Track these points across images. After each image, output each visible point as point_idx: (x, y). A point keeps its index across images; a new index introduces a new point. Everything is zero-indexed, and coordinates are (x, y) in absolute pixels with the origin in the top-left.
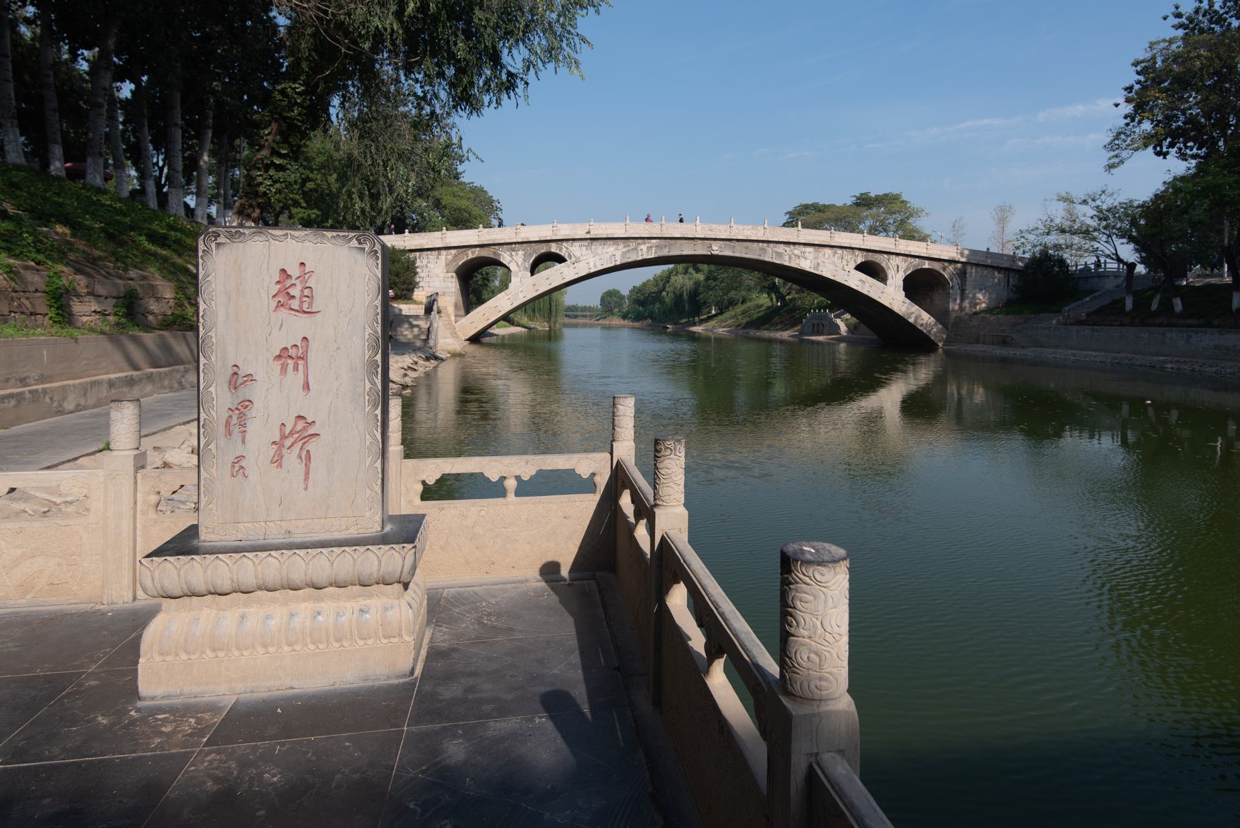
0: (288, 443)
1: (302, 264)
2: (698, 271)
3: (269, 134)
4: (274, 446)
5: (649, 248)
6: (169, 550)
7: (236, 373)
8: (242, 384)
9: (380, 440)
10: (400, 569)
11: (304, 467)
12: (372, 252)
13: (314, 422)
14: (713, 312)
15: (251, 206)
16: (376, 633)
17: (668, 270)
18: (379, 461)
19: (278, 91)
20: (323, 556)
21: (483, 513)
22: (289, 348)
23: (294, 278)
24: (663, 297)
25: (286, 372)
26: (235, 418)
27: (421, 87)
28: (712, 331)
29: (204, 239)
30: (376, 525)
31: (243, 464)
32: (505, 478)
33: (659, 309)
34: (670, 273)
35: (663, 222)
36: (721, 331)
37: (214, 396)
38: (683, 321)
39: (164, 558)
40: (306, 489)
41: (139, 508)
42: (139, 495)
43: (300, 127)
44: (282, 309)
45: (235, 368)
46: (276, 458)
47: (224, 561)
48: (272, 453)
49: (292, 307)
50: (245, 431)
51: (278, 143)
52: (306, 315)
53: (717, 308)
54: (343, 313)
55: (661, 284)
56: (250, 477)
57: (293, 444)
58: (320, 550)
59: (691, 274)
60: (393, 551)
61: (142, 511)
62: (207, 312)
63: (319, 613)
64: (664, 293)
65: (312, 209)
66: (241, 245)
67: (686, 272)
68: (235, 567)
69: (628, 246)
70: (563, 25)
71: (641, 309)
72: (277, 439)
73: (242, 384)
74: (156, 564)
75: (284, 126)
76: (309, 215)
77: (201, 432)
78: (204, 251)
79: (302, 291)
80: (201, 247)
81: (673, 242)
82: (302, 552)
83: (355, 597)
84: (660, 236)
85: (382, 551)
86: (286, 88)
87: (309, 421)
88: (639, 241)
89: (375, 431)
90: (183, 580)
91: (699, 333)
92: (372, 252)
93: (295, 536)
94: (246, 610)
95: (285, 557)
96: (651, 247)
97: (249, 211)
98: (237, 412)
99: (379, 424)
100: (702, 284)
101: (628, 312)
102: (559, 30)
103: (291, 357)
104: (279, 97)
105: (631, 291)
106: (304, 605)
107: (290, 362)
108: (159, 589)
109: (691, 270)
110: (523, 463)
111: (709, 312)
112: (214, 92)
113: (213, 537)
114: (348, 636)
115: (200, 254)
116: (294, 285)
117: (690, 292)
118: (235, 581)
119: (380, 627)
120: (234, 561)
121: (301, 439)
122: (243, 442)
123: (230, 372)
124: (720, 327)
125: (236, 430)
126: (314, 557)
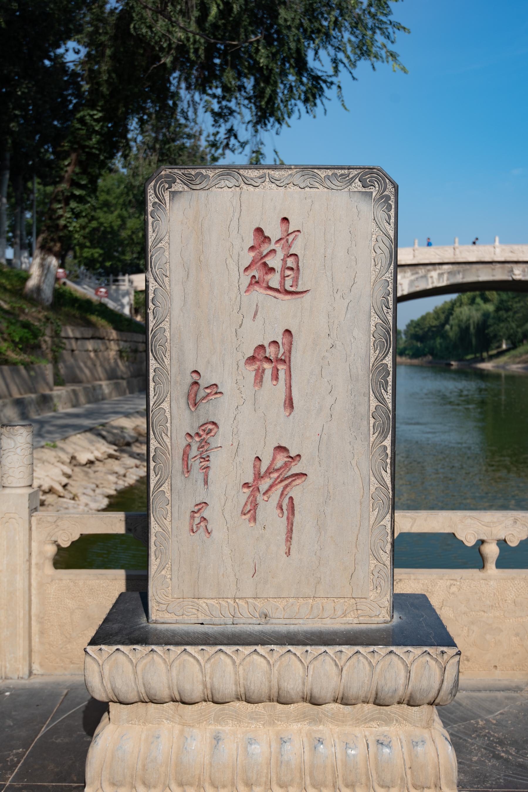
0: (264, 485)
1: (285, 220)
2: (486, 300)
3: (69, 165)
4: (245, 490)
5: (441, 275)
6: (117, 634)
7: (196, 383)
8: (204, 398)
9: (390, 485)
10: (436, 686)
11: (286, 522)
12: (382, 198)
13: (299, 456)
14: (504, 347)
15: (52, 240)
16: (402, 779)
17: (451, 302)
18: (388, 517)
19: (78, 119)
20: (327, 658)
21: (454, 589)
22: (266, 345)
23: (273, 241)
24: (446, 331)
25: (261, 381)
26: (194, 447)
27: (219, 102)
28: (503, 367)
29: (155, 186)
30: (384, 611)
31: (206, 513)
32: (482, 542)
33: (441, 344)
34: (453, 304)
35: (457, 245)
36: (515, 368)
37: (168, 415)
38: (469, 357)
39: (115, 647)
40: (288, 553)
41: (34, 561)
42: (34, 544)
43: (97, 156)
44: (256, 287)
45: (195, 376)
46: (248, 507)
47: (194, 657)
48: (243, 499)
49: (271, 285)
50: (208, 467)
51: (77, 174)
52: (288, 297)
53: (509, 342)
54: (340, 294)
55: (443, 317)
56: (214, 534)
57: (271, 487)
58: (323, 648)
59: (479, 304)
60: (428, 658)
61: (37, 564)
62: (158, 293)
63: (320, 741)
64: (447, 327)
65: (95, 248)
66: (202, 193)
67: (472, 302)
68: (208, 666)
69: (417, 273)
70: (374, 16)
71: (419, 344)
72: (250, 479)
73: (204, 398)
74: (105, 656)
75: (84, 158)
76: (92, 254)
77: (152, 467)
78: (155, 203)
79: (284, 260)
80: (151, 198)
81: (468, 267)
82: (298, 650)
83: (367, 720)
84: (452, 260)
85: (411, 656)
86: (84, 116)
87: (293, 454)
88: (430, 267)
89: (383, 472)
90: (141, 681)
91: (488, 370)
92: (382, 198)
93: (274, 621)
94: (219, 727)
95: (276, 655)
96: (442, 274)
97: (52, 244)
98: (197, 439)
99: (389, 461)
100: (492, 315)
101: (405, 349)
102: (370, 22)
103: (268, 360)
104: (78, 126)
105: (408, 326)
106: (296, 727)
107: (267, 366)
108: (109, 690)
109: (478, 300)
110: (510, 522)
111: (500, 346)
112: (11, 133)
113: (167, 617)
114: (364, 780)
115: (150, 208)
116: (273, 251)
117: (478, 324)
118: (209, 686)
119: (409, 771)
120: (207, 657)
121: (282, 481)
122: (206, 482)
123: (189, 380)
124: (514, 363)
125: (196, 465)
126: (316, 658)
